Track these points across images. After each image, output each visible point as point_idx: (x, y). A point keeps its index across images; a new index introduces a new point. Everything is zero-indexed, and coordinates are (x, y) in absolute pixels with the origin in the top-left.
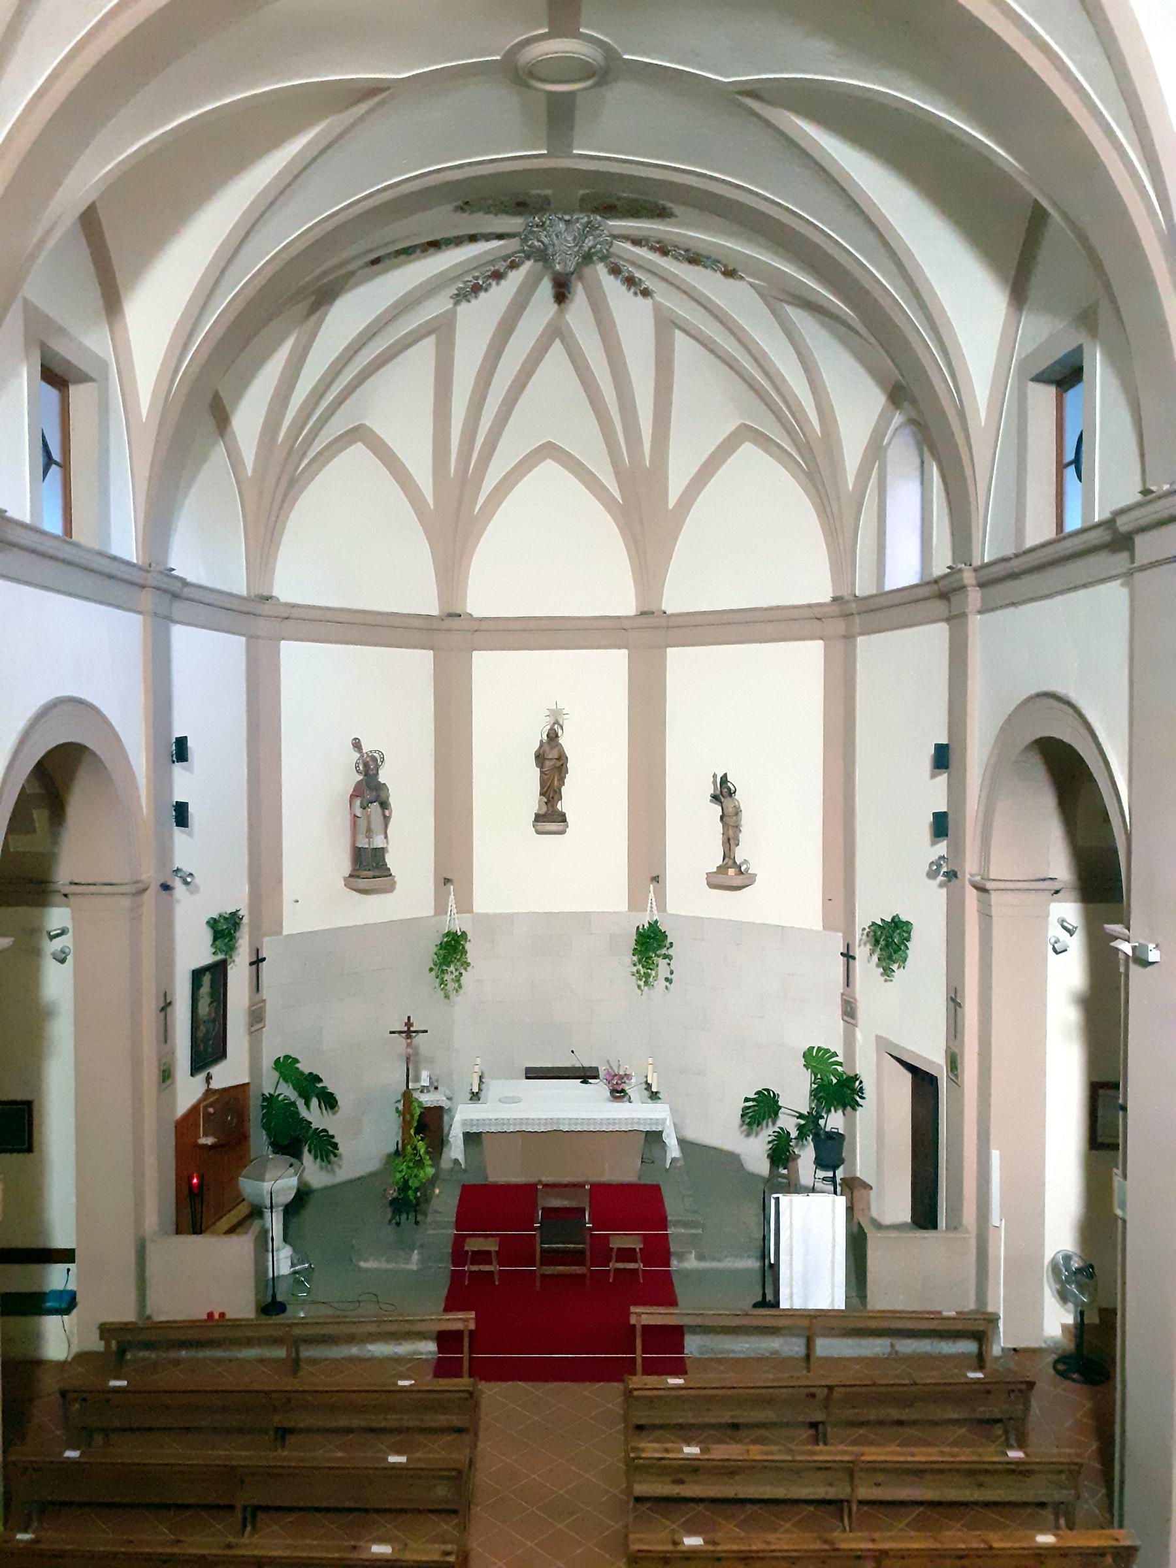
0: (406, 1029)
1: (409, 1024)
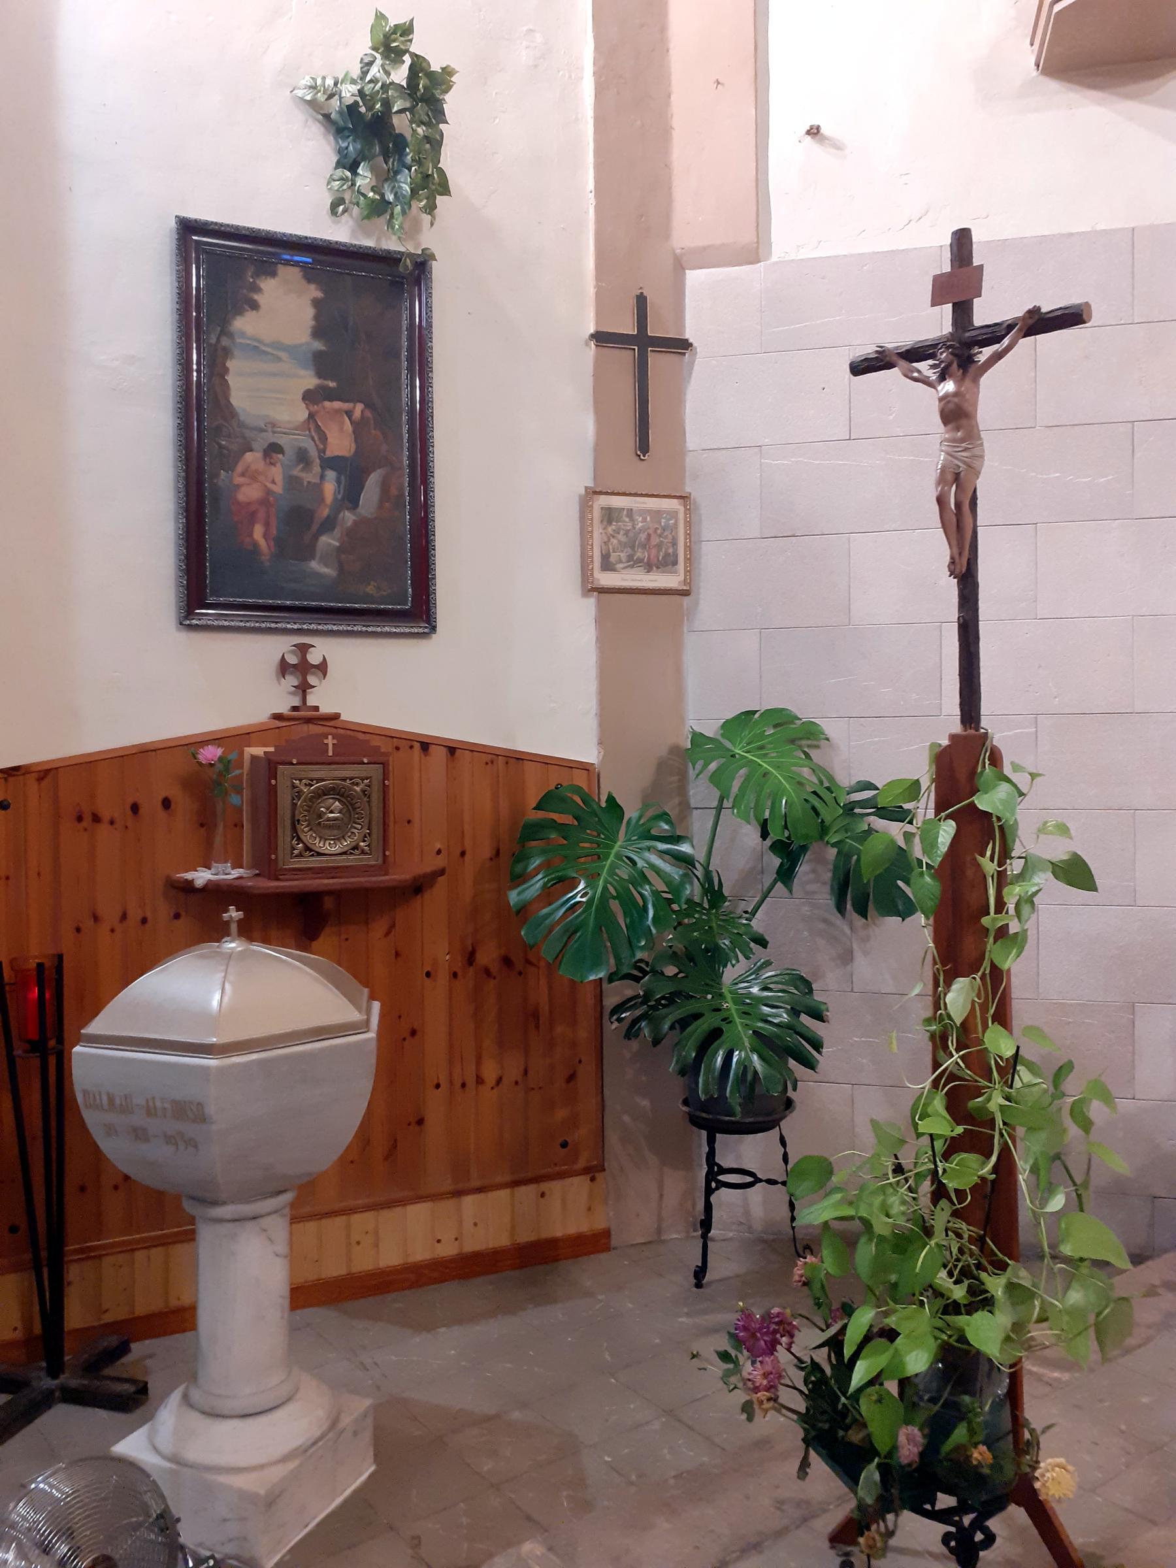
0: (937, 323)
1: (959, 279)
